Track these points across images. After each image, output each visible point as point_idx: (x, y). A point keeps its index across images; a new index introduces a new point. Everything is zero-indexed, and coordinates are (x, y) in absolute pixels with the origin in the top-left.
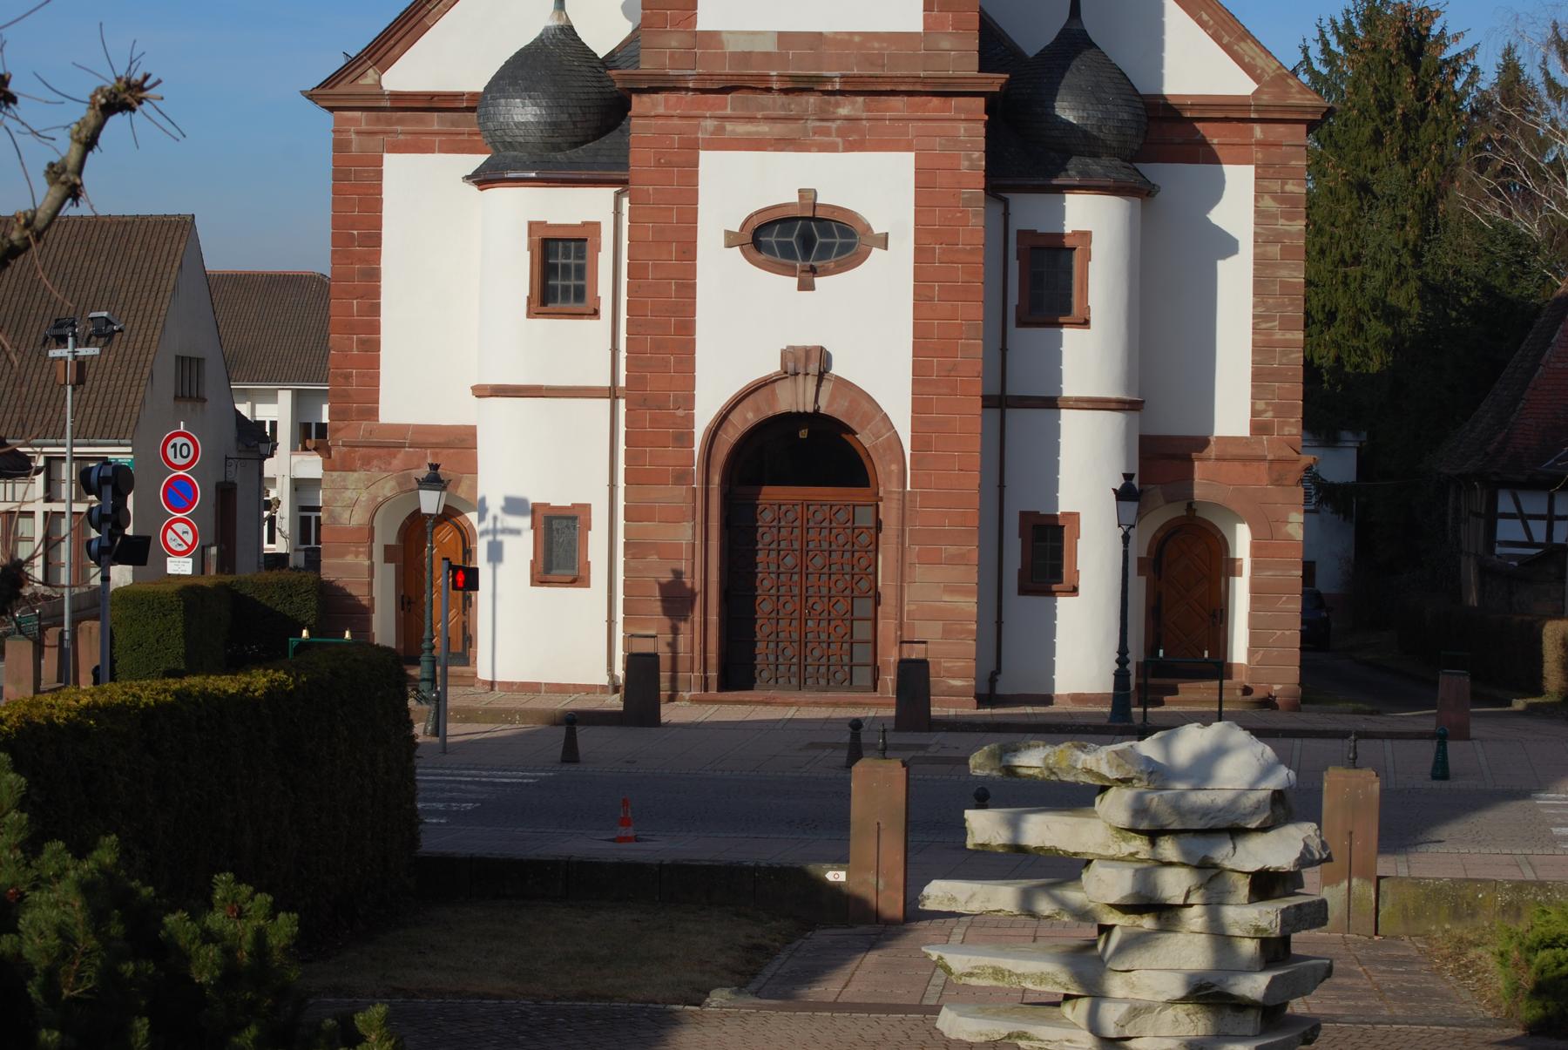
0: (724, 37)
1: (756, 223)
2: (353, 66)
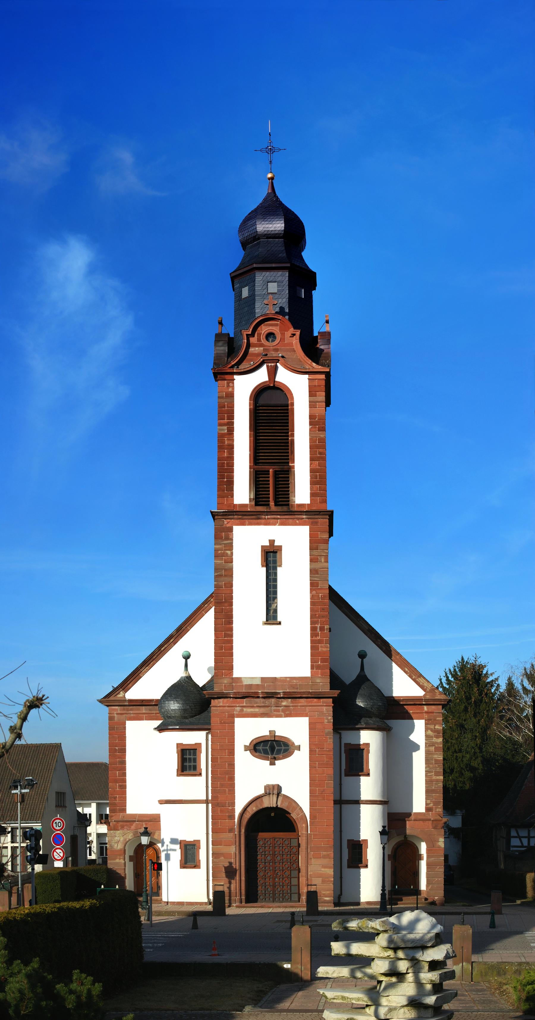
0: (243, 679)
1: (255, 742)
2: (115, 691)
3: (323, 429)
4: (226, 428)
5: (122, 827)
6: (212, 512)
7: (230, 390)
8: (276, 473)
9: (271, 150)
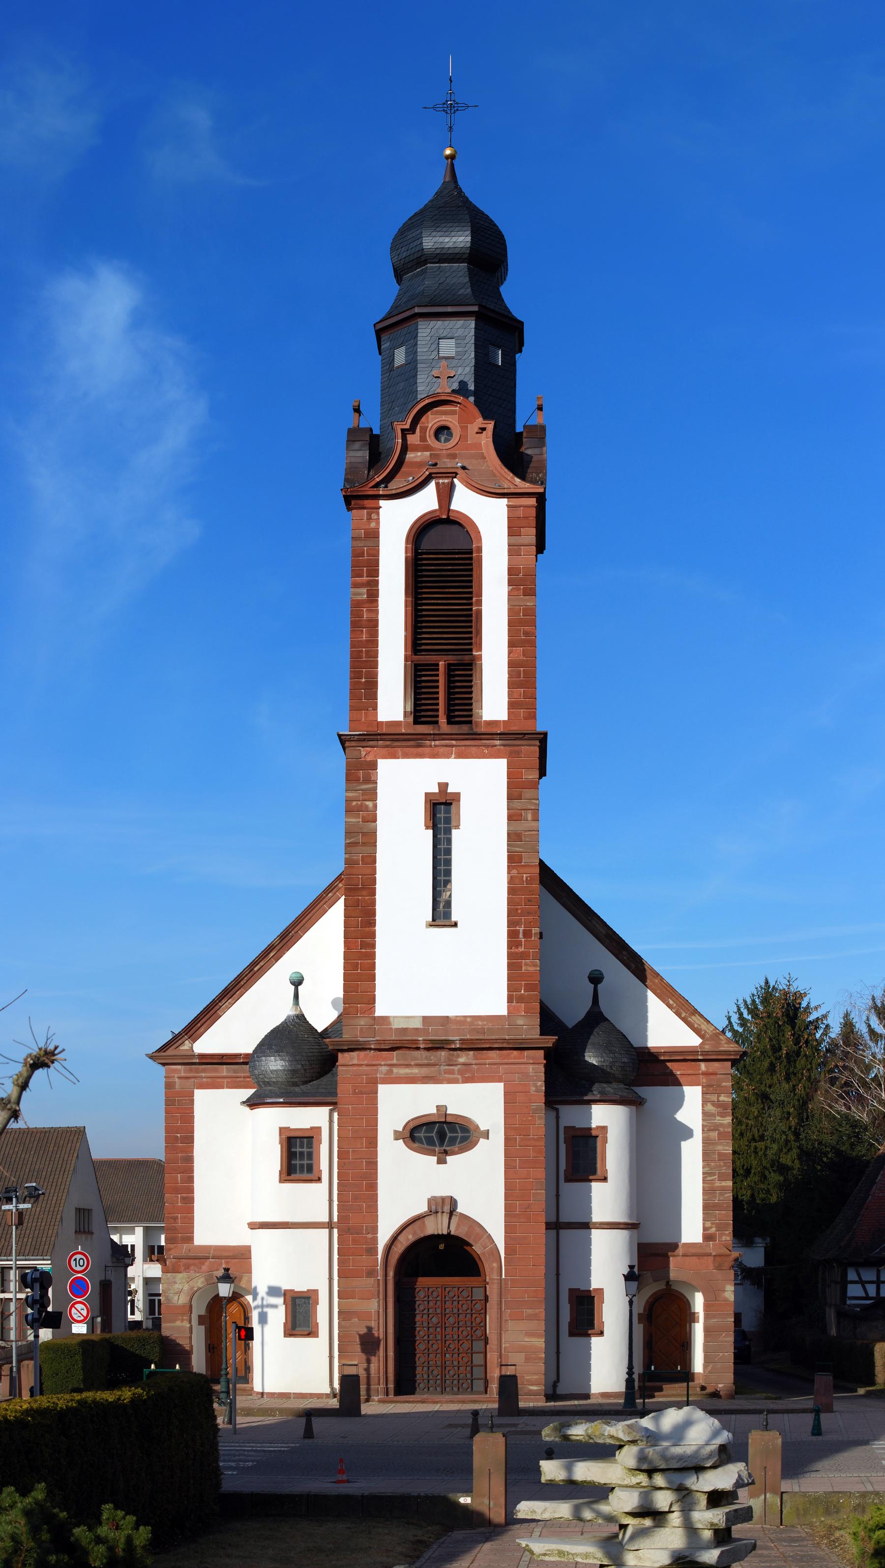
0: (391, 1019)
1: (412, 1126)
2: (176, 1039)
3: (531, 592)
4: (364, 590)
7: (373, 525)
8: (450, 667)
9: (451, 108)
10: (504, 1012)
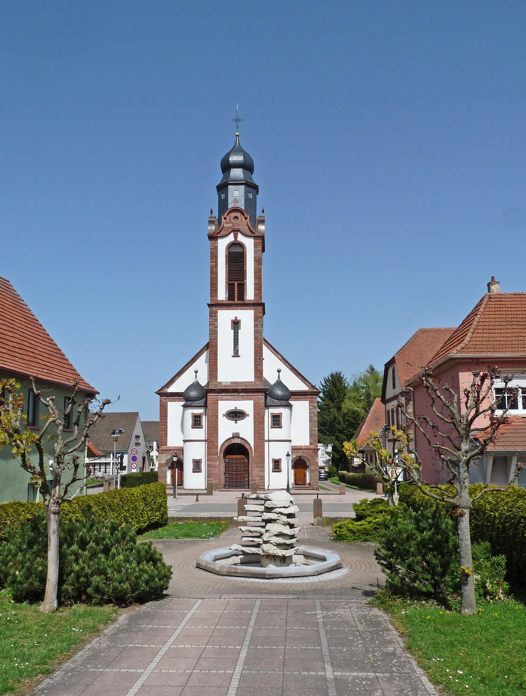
1: (228, 412)
2: (163, 388)
3: (260, 264)
4: (214, 263)
5: (165, 452)
6: (208, 304)
7: (216, 245)
8: (238, 284)
9: (237, 120)
10: (254, 381)
